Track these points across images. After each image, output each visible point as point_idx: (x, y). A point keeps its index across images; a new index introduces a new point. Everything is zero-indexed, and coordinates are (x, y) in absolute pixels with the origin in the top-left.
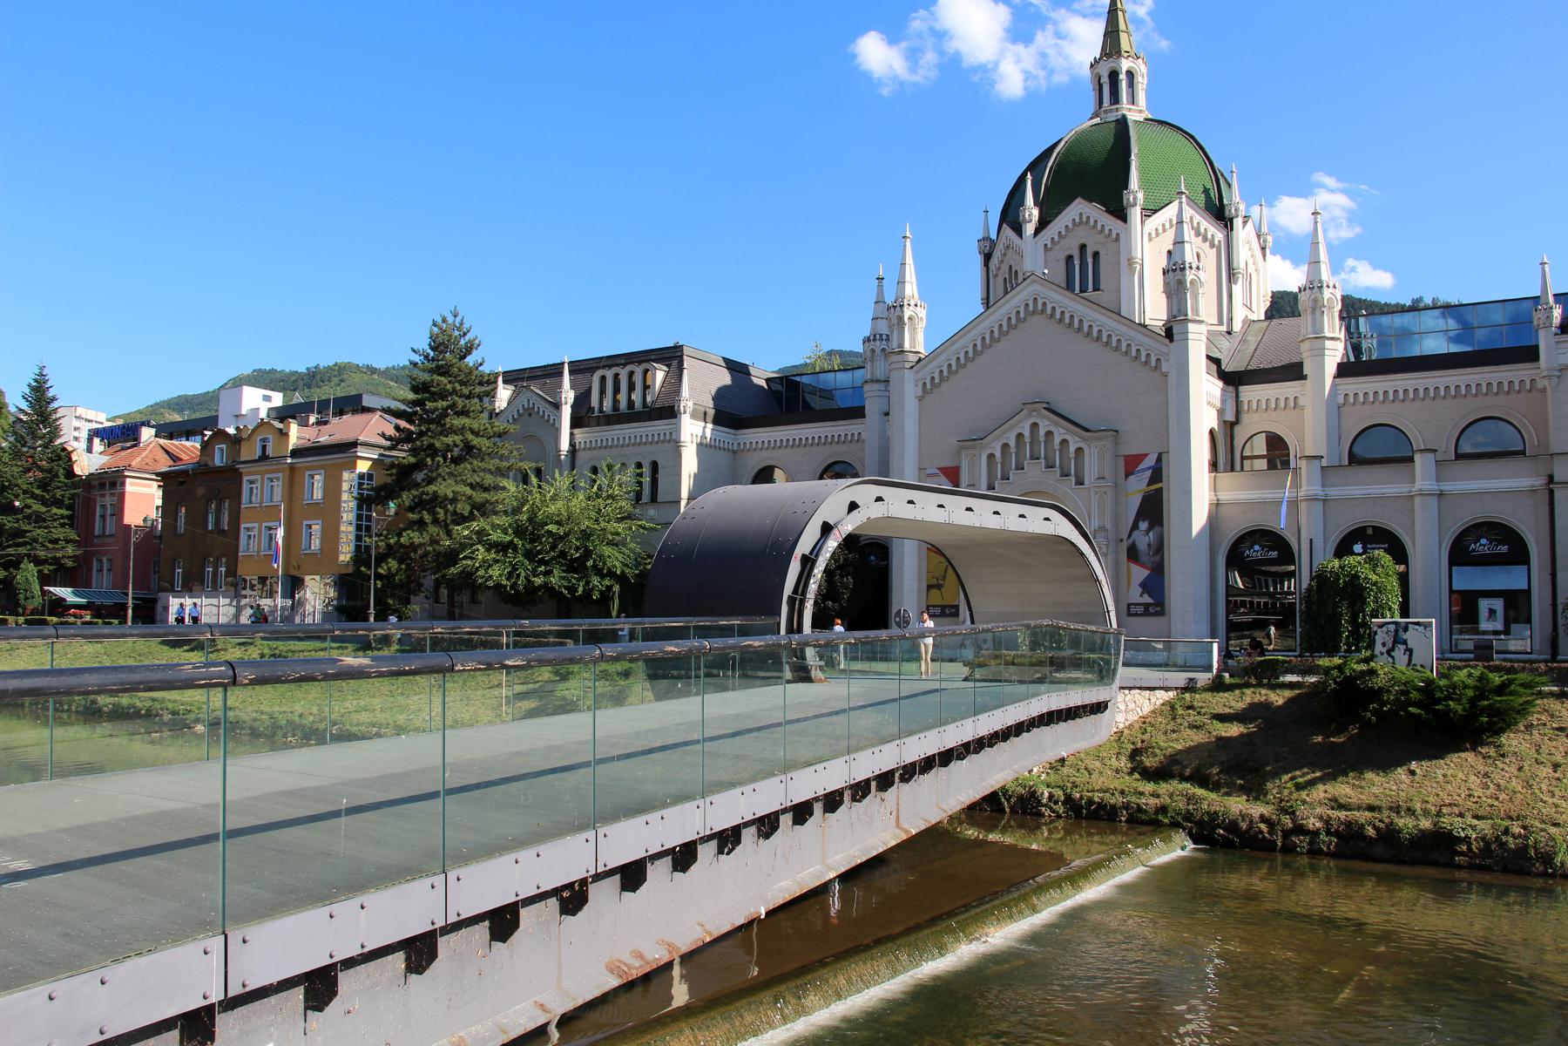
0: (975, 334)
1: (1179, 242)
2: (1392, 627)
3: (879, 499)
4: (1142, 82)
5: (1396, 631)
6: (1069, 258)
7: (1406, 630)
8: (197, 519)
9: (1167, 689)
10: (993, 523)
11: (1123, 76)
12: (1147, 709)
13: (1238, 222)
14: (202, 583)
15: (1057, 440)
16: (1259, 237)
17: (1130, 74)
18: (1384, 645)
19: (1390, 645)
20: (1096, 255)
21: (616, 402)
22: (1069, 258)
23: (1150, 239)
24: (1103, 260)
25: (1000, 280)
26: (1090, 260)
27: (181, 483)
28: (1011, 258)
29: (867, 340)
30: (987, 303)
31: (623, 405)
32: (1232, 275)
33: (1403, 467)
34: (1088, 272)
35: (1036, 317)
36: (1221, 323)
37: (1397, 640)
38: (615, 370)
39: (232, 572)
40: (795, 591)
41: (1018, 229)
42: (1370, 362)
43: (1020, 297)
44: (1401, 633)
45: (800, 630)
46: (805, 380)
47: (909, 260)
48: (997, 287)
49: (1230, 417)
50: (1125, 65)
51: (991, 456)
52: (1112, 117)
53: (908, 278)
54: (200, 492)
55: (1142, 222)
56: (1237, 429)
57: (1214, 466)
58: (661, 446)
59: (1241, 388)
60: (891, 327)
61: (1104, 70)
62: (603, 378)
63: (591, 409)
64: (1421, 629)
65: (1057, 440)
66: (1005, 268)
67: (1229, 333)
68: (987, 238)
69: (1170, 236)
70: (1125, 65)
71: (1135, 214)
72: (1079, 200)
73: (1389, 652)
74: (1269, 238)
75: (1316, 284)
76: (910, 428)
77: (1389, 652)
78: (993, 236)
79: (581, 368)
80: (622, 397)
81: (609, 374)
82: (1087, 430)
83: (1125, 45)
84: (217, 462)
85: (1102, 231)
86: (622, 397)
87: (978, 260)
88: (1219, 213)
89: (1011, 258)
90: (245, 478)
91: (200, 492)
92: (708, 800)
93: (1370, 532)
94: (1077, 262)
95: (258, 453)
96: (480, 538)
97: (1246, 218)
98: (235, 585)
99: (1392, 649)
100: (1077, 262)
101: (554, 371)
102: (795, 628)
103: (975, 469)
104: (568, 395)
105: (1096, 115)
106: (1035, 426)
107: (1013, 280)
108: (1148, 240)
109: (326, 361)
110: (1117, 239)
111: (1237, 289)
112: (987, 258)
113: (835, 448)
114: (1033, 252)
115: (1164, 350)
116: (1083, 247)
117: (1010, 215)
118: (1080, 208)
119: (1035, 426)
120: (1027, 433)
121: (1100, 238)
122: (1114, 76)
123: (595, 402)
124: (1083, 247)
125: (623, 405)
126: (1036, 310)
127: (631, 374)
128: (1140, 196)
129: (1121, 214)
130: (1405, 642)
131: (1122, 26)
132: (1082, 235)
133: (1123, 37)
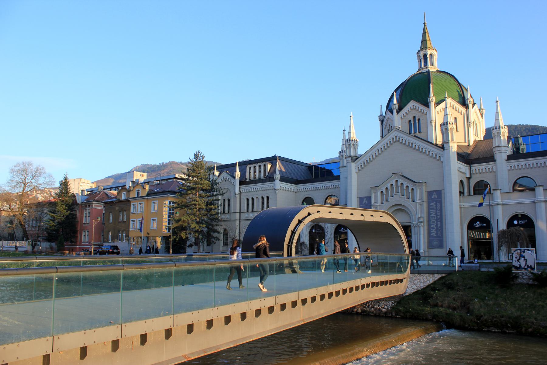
0: (378, 147)
1: (446, 115)
2: (519, 251)
3: (318, 212)
4: (435, 57)
5: (521, 253)
6: (410, 121)
7: (524, 252)
8: (116, 218)
9: (433, 273)
10: (362, 219)
11: (428, 56)
12: (431, 281)
13: (470, 106)
14: (117, 239)
15: (405, 186)
16: (480, 110)
17: (431, 55)
18: (516, 258)
19: (518, 258)
20: (419, 119)
21: (254, 175)
22: (410, 121)
23: (438, 113)
24: (421, 121)
25: (386, 130)
26: (417, 122)
27: (111, 206)
28: (390, 122)
29: (340, 152)
30: (382, 137)
31: (257, 177)
32: (469, 124)
33: (530, 193)
34: (416, 127)
35: (396, 143)
36: (465, 142)
37: (521, 256)
38: (254, 165)
39: (127, 236)
40: (289, 243)
41: (391, 112)
42: (523, 154)
43: (393, 134)
44: (522, 253)
45: (291, 256)
46: (320, 166)
47: (352, 125)
48: (385, 131)
49: (468, 176)
50: (429, 52)
51: (382, 192)
52: (424, 71)
53: (352, 131)
54: (117, 208)
55: (435, 108)
56: (471, 180)
57: (462, 193)
58: (270, 191)
59: (472, 165)
60: (346, 148)
61: (421, 54)
62: (250, 168)
63: (246, 179)
64: (530, 252)
65: (405, 186)
66: (388, 126)
67: (468, 145)
68: (382, 115)
69: (443, 113)
70: (429, 52)
71: (432, 105)
72: (412, 101)
73: (518, 260)
74: (484, 111)
75: (498, 127)
76: (353, 182)
77: (518, 260)
78: (384, 114)
79: (243, 164)
80: (257, 173)
81: (252, 166)
82: (415, 182)
83: (429, 45)
84: (123, 199)
85: (421, 112)
86: (257, 173)
87: (379, 123)
88: (463, 102)
89: (390, 122)
90: (132, 204)
91: (117, 208)
92: (216, 308)
93: (520, 216)
94: (412, 123)
95: (136, 196)
96: (202, 223)
97: (474, 104)
98: (128, 240)
99: (519, 259)
100: (412, 123)
101: (235, 165)
102: (289, 254)
103: (376, 198)
104: (238, 174)
105: (419, 70)
106: (397, 181)
107: (391, 128)
108: (436, 114)
109: (166, 161)
110: (426, 114)
111: (471, 130)
112: (382, 122)
113: (306, 193)
114: (397, 120)
115: (441, 153)
116: (414, 117)
117: (389, 108)
118: (412, 104)
119: (397, 181)
120: (394, 184)
121: (420, 114)
122: (425, 56)
123: (248, 176)
124: (414, 117)
125: (257, 177)
126: (397, 141)
127: (255, 167)
128: (434, 98)
129: (427, 105)
130: (524, 257)
131: (427, 38)
132: (414, 113)
133: (428, 42)
